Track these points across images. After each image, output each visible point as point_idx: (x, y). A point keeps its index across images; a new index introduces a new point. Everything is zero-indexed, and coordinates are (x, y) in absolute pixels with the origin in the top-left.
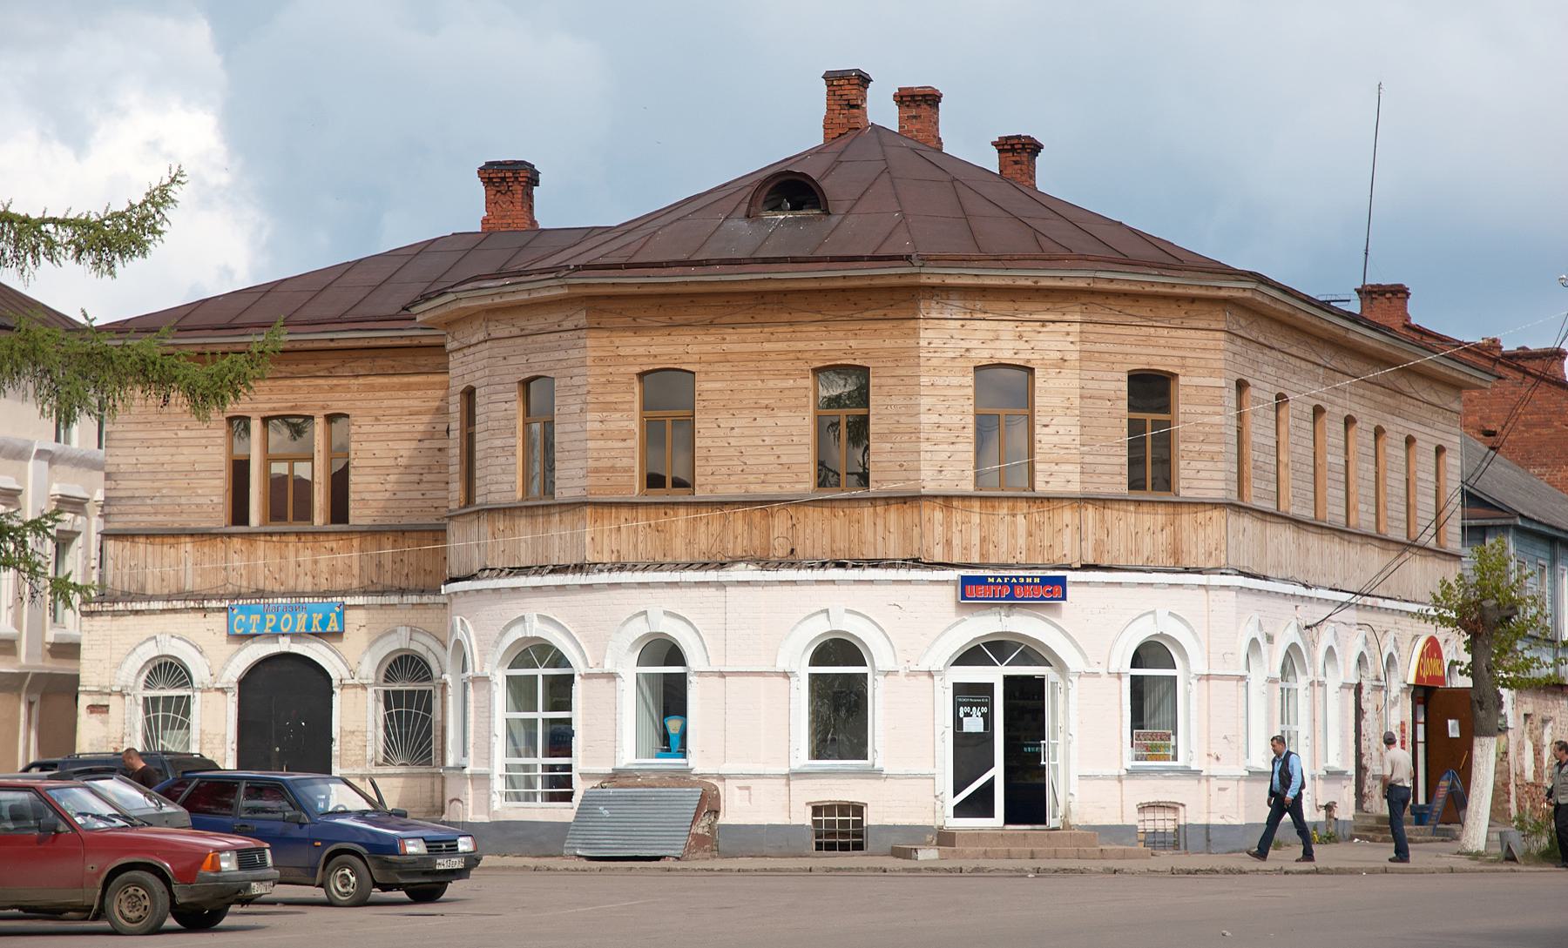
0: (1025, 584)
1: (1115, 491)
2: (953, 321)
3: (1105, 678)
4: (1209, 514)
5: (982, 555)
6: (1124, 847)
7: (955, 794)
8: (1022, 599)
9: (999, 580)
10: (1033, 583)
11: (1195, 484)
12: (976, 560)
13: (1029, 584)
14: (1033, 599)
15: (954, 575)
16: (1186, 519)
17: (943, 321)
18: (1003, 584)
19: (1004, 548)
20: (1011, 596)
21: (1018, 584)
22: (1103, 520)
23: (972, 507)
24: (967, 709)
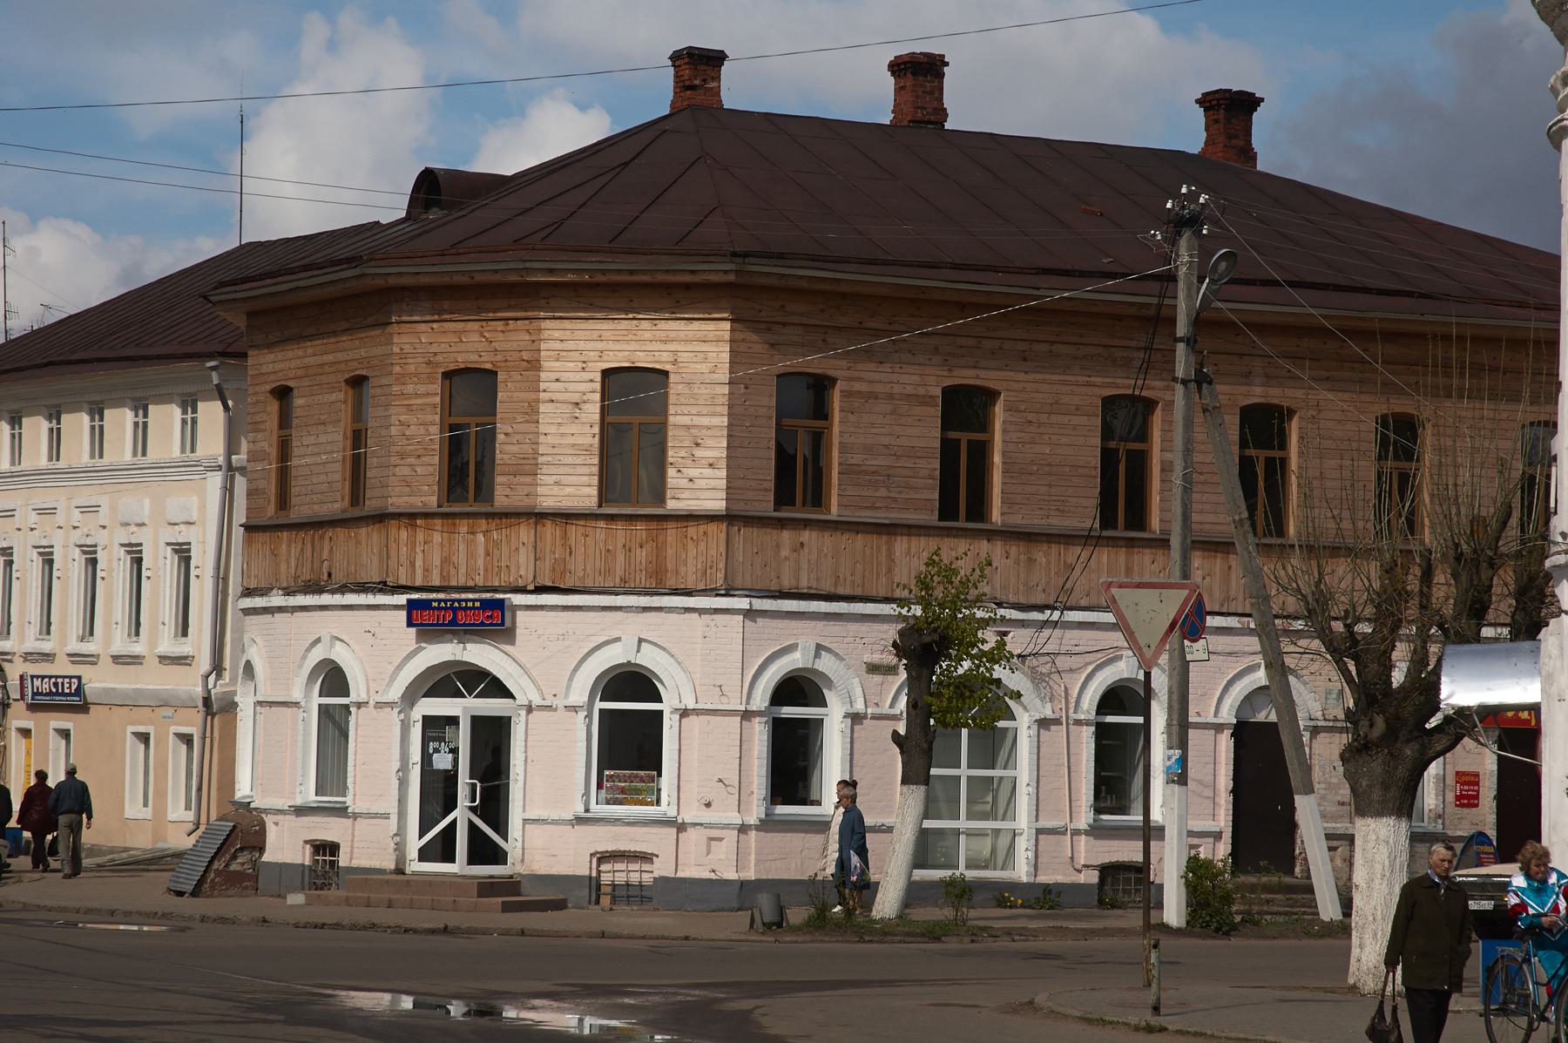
0: (467, 608)
1: (576, 504)
2: (423, 325)
3: (561, 712)
4: (702, 528)
5: (442, 576)
6: (1329, 904)
7: (421, 837)
8: (464, 625)
9: (443, 604)
10: (473, 608)
11: (686, 495)
12: (436, 582)
13: (470, 609)
14: (474, 625)
15: (401, 599)
16: (672, 533)
17: (414, 325)
18: (446, 609)
19: (463, 570)
20: (453, 622)
21: (460, 608)
22: (565, 536)
23: (435, 524)
24: (436, 745)
